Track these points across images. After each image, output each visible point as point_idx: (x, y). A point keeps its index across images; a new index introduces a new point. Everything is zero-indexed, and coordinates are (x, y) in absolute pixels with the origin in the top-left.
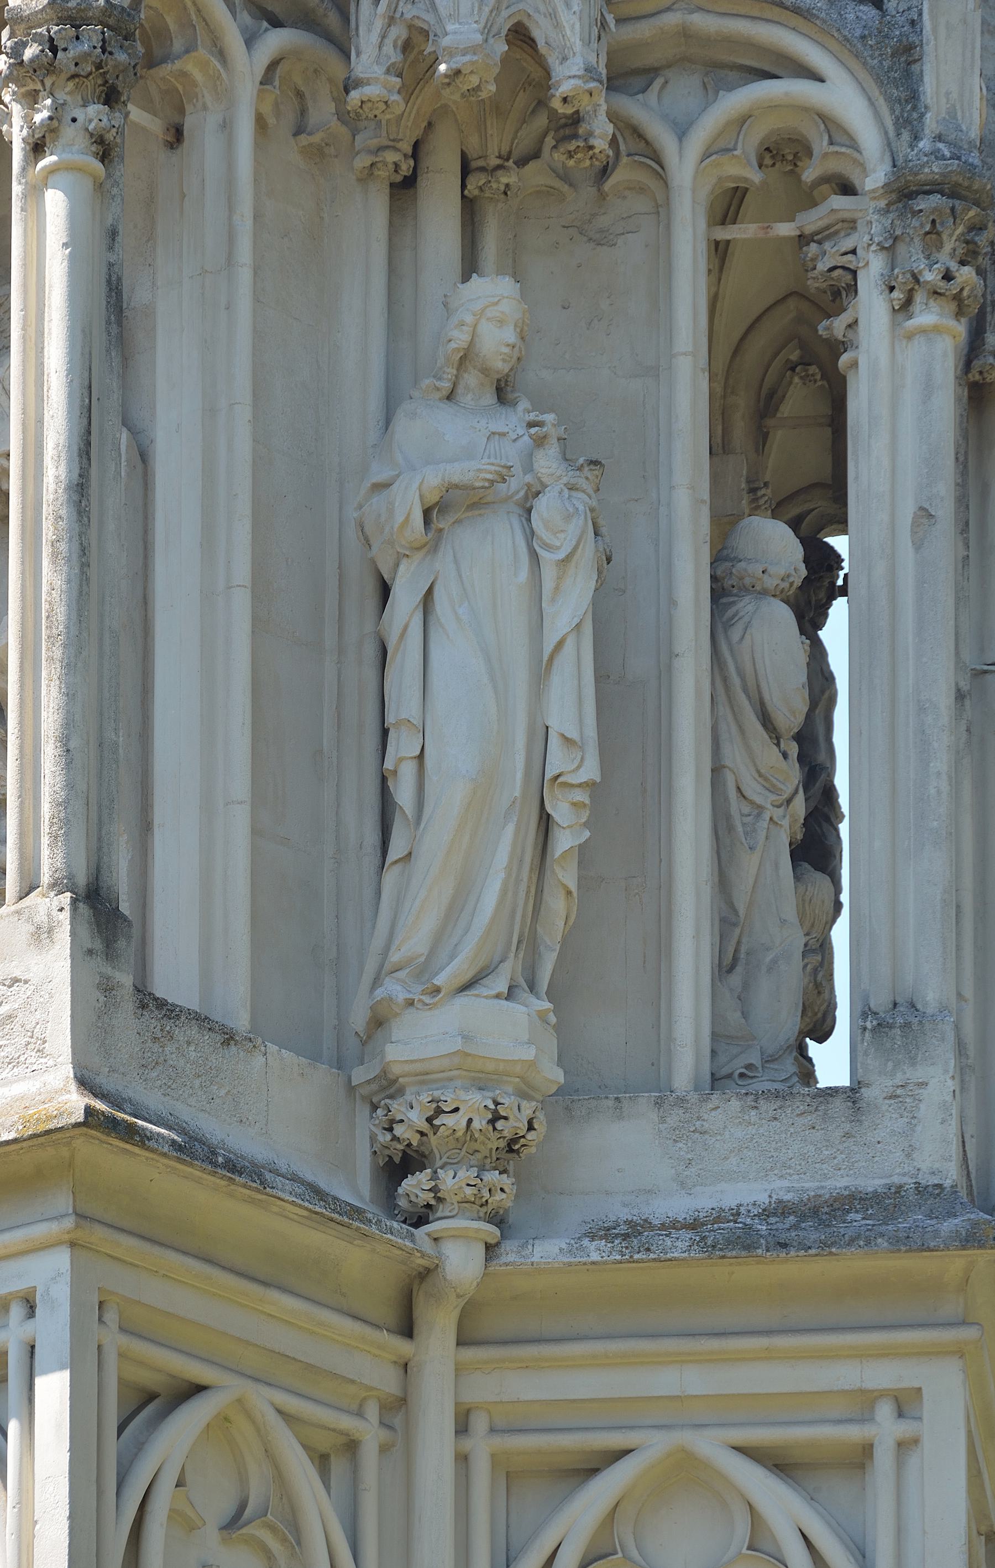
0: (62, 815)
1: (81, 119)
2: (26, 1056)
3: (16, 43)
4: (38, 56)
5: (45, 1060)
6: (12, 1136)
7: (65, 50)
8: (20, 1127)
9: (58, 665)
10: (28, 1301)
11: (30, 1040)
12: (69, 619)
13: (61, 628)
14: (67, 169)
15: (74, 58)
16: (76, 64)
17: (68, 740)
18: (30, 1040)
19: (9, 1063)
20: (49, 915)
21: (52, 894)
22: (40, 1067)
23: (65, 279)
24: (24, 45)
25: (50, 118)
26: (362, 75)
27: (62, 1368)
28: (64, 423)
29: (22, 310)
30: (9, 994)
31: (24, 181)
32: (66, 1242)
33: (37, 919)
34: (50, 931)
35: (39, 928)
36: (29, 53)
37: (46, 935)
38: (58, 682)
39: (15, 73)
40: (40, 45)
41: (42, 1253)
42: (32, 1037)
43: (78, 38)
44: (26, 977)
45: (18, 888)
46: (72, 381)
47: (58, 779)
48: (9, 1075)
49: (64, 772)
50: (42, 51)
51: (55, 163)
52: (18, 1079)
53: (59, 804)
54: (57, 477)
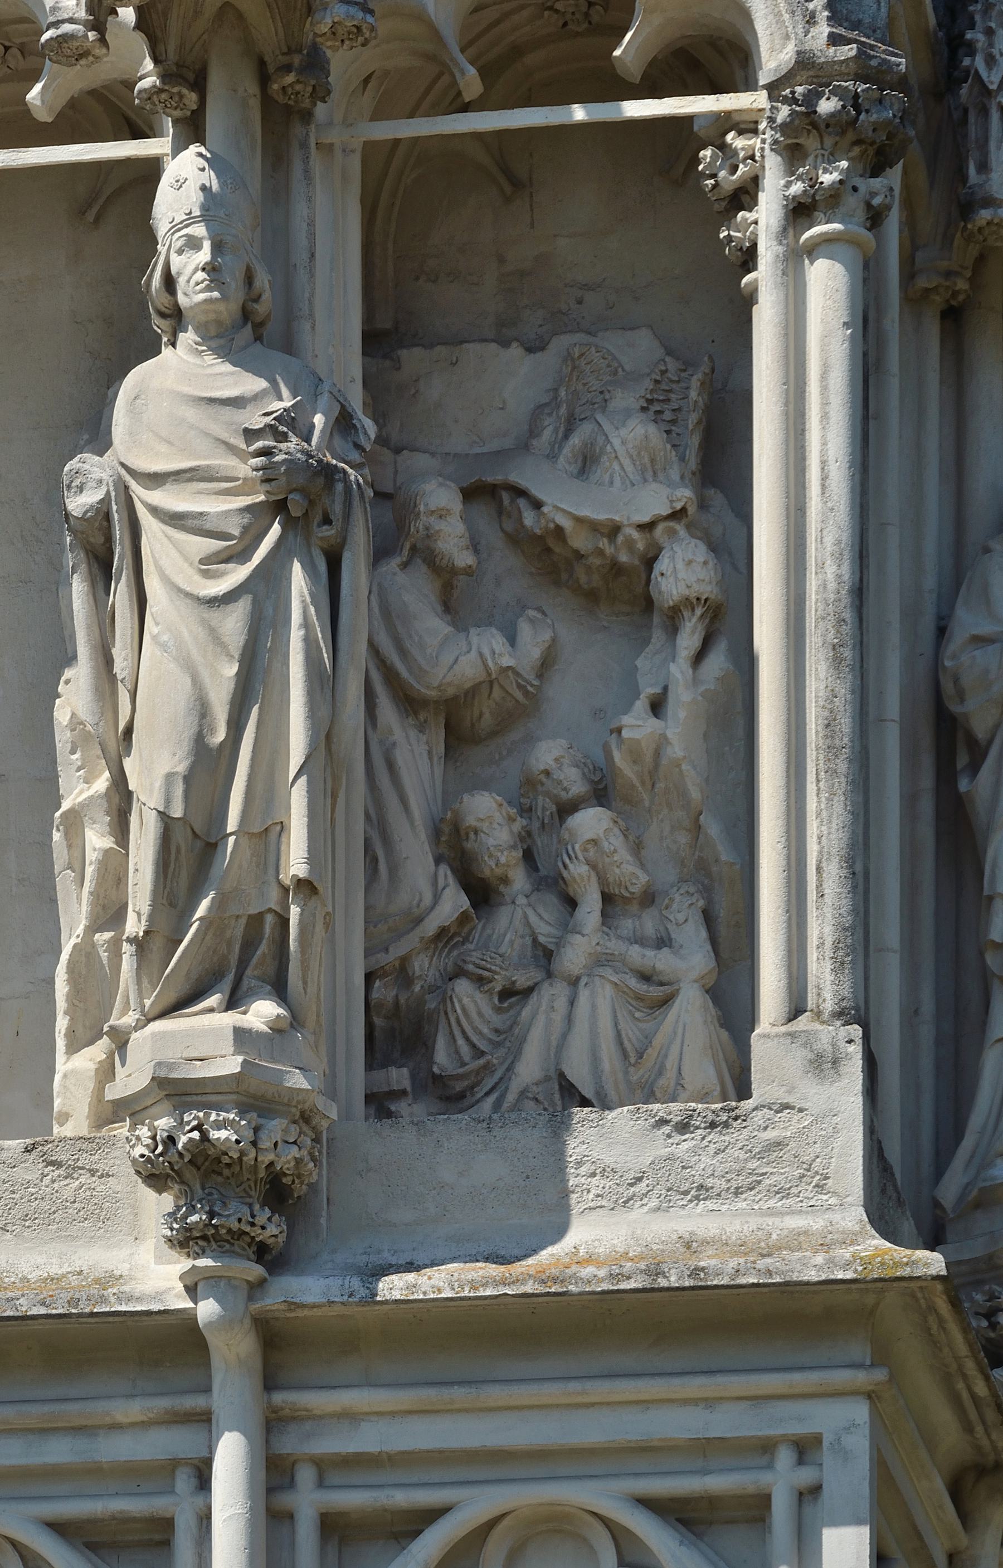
0: (849, 941)
1: (863, 188)
2: (800, 1189)
3: (809, 91)
4: (839, 111)
5: (825, 1197)
6: (849, 1275)
7: (867, 111)
8: (860, 1268)
9: (843, 780)
10: (798, 1446)
11: (806, 1173)
12: (853, 732)
13: (846, 740)
14: (848, 241)
15: (874, 123)
16: (874, 130)
17: (854, 863)
18: (806, 1173)
19: (777, 1193)
20: (834, 1045)
21: (838, 1023)
22: (819, 1203)
23: (846, 362)
24: (820, 95)
25: (841, 182)
26: (996, 195)
27: (859, 1522)
28: (847, 519)
29: (784, 384)
30: (776, 1119)
31: (785, 242)
32: (863, 1393)
33: (818, 1046)
34: (835, 1062)
35: (820, 1056)
36: (826, 106)
37: (829, 1065)
38: (843, 798)
39: (797, 122)
40: (840, 99)
41: (830, 1400)
42: (808, 1170)
43: (880, 102)
44: (803, 1105)
45: (787, 1009)
46: (853, 475)
47: (844, 902)
48: (780, 1204)
49: (850, 895)
50: (844, 107)
51: (840, 232)
52: (791, 1212)
53: (845, 929)
54: (839, 576)
